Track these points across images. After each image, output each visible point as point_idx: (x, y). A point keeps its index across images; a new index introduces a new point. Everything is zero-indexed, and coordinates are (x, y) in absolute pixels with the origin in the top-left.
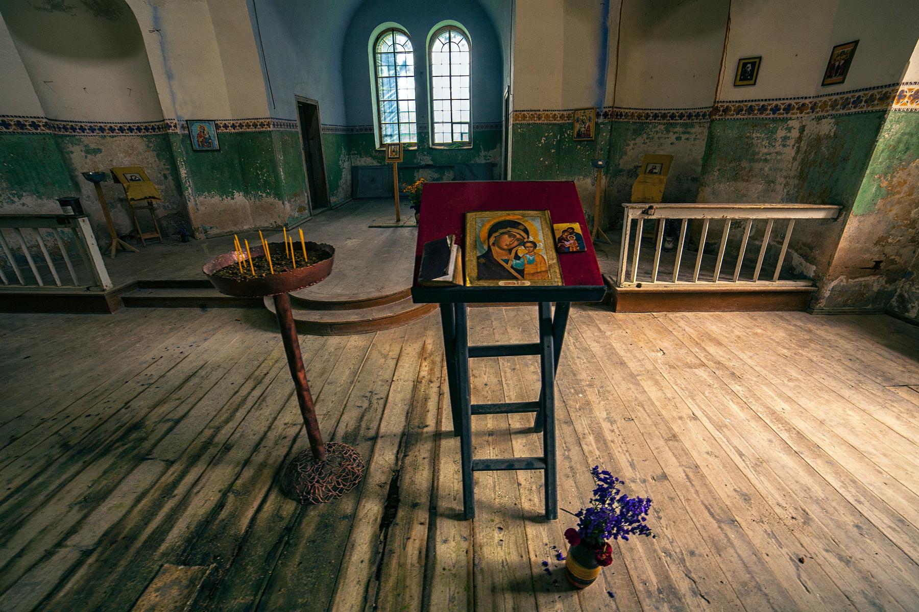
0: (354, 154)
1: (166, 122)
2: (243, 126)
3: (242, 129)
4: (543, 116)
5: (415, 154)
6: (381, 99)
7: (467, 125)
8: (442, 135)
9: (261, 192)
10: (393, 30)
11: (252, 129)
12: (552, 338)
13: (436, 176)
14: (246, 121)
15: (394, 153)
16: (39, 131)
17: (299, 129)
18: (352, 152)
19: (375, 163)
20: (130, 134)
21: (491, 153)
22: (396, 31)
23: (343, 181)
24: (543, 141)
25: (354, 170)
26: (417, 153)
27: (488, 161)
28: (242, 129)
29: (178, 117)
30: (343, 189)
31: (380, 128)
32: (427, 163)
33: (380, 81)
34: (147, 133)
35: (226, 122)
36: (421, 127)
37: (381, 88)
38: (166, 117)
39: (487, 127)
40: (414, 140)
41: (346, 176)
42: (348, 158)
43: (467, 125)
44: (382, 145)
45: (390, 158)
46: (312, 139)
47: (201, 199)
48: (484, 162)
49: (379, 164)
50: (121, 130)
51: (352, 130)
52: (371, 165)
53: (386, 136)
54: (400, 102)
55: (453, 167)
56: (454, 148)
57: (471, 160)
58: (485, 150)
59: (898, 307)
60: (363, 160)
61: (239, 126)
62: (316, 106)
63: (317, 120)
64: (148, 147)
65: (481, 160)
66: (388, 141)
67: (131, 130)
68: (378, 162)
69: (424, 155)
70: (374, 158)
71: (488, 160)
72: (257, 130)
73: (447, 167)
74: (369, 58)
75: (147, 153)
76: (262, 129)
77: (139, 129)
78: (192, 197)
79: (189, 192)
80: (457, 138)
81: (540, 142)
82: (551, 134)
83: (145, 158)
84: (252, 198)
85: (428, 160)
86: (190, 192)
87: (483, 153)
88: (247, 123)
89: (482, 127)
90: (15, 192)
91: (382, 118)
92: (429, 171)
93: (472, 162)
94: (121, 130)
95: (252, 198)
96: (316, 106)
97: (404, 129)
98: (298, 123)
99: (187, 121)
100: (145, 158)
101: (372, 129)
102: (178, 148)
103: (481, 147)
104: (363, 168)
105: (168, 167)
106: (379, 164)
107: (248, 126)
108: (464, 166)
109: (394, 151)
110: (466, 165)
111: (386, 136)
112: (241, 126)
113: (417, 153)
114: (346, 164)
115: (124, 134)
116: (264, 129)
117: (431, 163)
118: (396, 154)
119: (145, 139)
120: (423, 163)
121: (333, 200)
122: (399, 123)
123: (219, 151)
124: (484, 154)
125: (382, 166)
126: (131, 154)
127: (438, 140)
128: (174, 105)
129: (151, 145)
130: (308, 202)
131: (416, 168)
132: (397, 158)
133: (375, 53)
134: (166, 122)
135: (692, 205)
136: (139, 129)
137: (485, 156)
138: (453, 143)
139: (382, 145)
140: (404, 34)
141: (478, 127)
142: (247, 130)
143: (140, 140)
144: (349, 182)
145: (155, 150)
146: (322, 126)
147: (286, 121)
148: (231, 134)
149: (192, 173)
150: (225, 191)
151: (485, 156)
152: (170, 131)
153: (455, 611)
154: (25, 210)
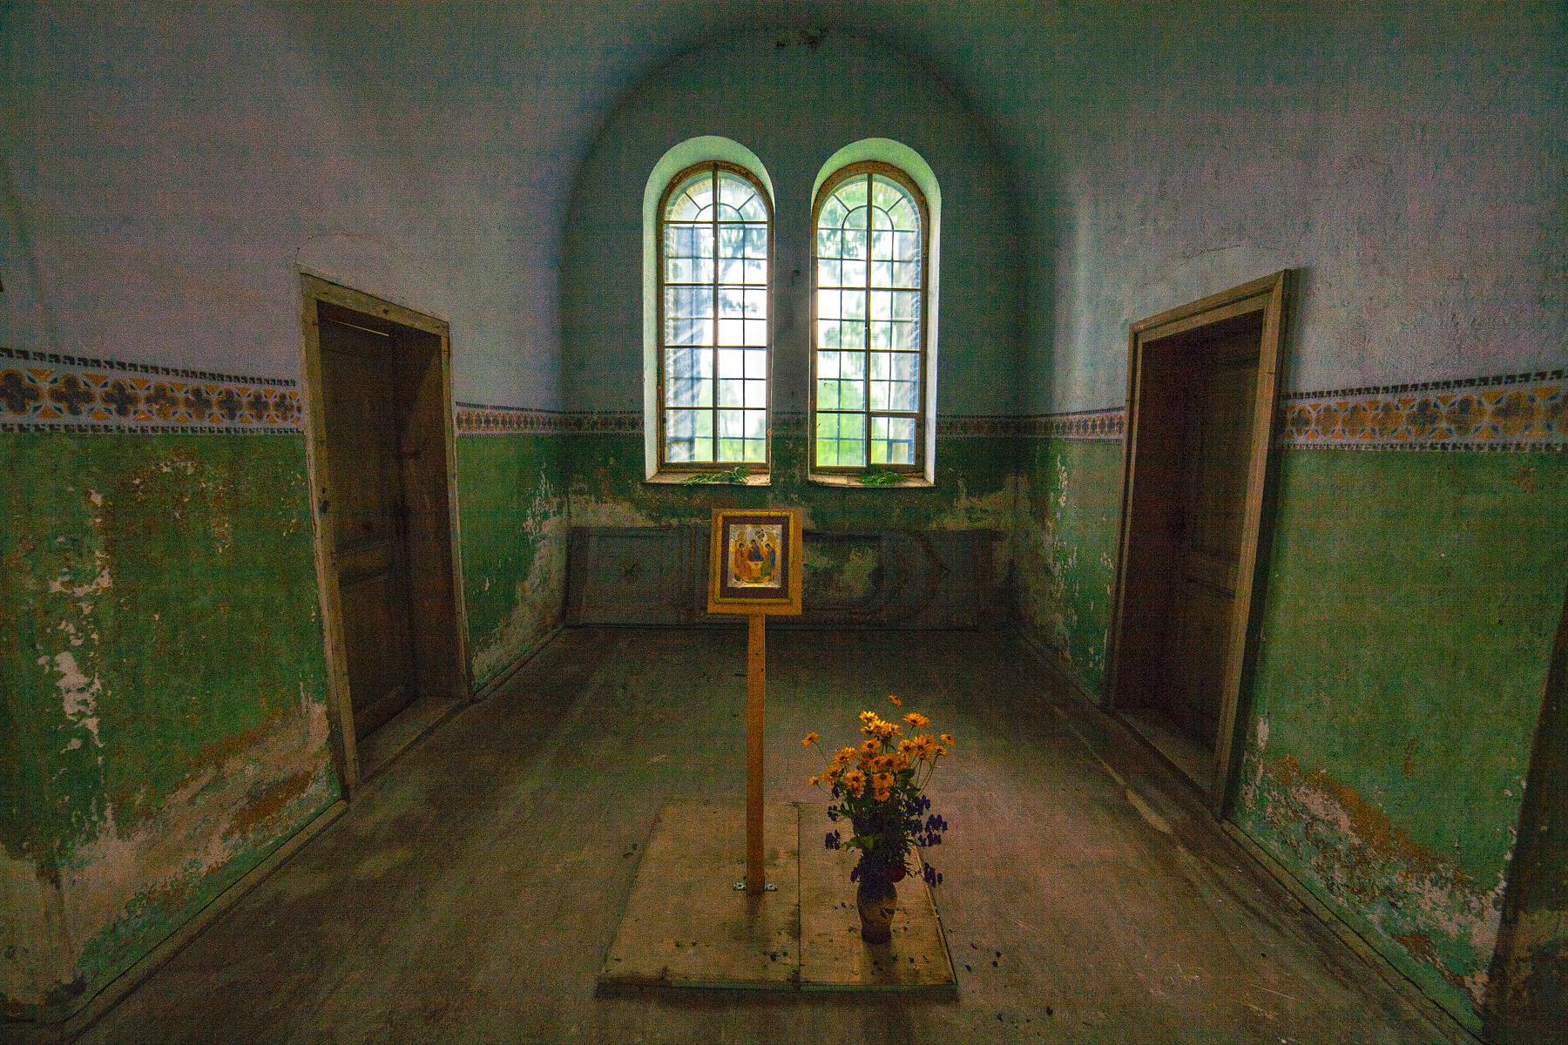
0: (581, 492)
4: (1444, 409)
6: (670, 340)
10: (716, 167)
12: (777, 586)
17: (306, 422)
18: (576, 486)
19: (641, 521)
21: (988, 502)
22: (724, 168)
23: (534, 579)
25: (577, 539)
27: (978, 525)
30: (533, 606)
31: (662, 420)
33: (670, 294)
35: (80, 373)
37: (670, 313)
40: (757, 454)
41: (548, 559)
42: (560, 506)
44: (664, 467)
46: (415, 455)
48: (964, 525)
49: (651, 524)
51: (579, 423)
52: (628, 525)
53: (677, 440)
54: (720, 352)
55: (878, 538)
57: (928, 519)
58: (969, 494)
60: (605, 509)
62: (438, 338)
63: (439, 388)
65: (954, 522)
66: (679, 455)
68: (650, 516)
70: (638, 505)
71: (979, 519)
74: (645, 264)
80: (880, 456)
87: (964, 502)
89: (965, 427)
91: (670, 394)
96: (438, 338)
97: (730, 425)
98: (304, 393)
101: (638, 423)
103: (960, 483)
104: (607, 533)
106: (651, 524)
109: (755, 555)
110: (919, 535)
111: (677, 440)
114: (551, 526)
118: (766, 573)
121: (484, 662)
122: (715, 409)
124: (968, 504)
125: (661, 529)
127: (826, 456)
128: (839, 429)
130: (335, 739)
133: (660, 223)
137: (970, 511)
138: (871, 470)
139: (664, 467)
140: (747, 175)
141: (951, 426)
144: (555, 583)
146: (456, 410)
151: (970, 511)
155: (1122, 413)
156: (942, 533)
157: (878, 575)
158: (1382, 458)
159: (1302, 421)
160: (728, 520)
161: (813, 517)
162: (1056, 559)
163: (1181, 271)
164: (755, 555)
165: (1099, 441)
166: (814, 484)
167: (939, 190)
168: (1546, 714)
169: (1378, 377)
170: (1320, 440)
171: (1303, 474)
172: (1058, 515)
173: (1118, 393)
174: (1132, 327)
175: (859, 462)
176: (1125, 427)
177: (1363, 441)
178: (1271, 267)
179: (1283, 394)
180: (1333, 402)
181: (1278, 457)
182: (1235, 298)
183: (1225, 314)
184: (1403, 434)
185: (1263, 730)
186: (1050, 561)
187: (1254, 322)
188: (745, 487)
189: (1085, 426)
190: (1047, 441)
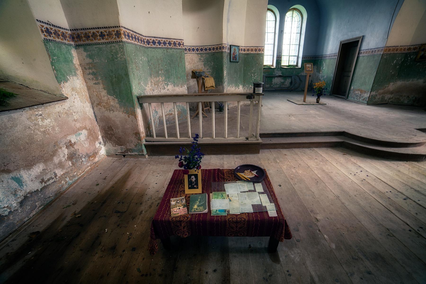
1: (223, 45)
2: (249, 50)
3: (248, 51)
5: (274, 70)
7: (296, 57)
8: (285, 63)
9: (251, 86)
11: (254, 52)
13: (282, 81)
14: (251, 48)
15: (309, 68)
16: (166, 46)
20: (193, 52)
24: (395, 62)
26: (275, 70)
28: (248, 51)
29: (227, 43)
32: (279, 75)
34: (201, 52)
36: (278, 57)
38: (224, 43)
39: (309, 58)
43: (296, 57)
45: (307, 71)
47: (229, 88)
50: (189, 50)
55: (291, 77)
56: (292, 69)
57: (299, 73)
59: (59, 177)
61: (247, 50)
64: (200, 59)
67: (193, 50)
69: (278, 71)
72: (256, 52)
73: (288, 77)
75: (199, 63)
76: (259, 52)
77: (197, 50)
78: (226, 87)
79: (225, 84)
81: (393, 62)
82: (400, 58)
83: (197, 66)
84: (246, 89)
85: (280, 73)
86: (226, 84)
88: (252, 49)
89: (306, 58)
90: (166, 82)
92: (279, 78)
93: (300, 74)
94: (189, 50)
95: (246, 89)
99: (230, 46)
100: (197, 66)
102: (226, 60)
105: (210, 70)
107: (252, 50)
108: (296, 77)
109: (309, 67)
110: (298, 76)
112: (248, 50)
113: (275, 70)
115: (190, 52)
116: (260, 52)
117: (281, 75)
119: (199, 55)
120: (277, 75)
123: (238, 62)
126: (191, 63)
129: (202, 58)
131: (273, 77)
132: (310, 71)
134: (223, 45)
135: (342, 97)
136: (197, 50)
141: (304, 58)
142: (251, 52)
143: (196, 55)
145: (203, 61)
147: (135, 34)
148: (243, 54)
149: (228, 74)
150: (237, 86)
152: (224, 50)
153: (356, 279)
154: (168, 93)
155: (337, 54)
156: (301, 75)
157: (291, 83)
158: (368, 56)
159: (361, 53)
160: (311, 64)
161: (282, 73)
162: (322, 78)
163: (349, 34)
164: (309, 67)
165: (332, 58)
166: (282, 68)
167: (375, 73)
168: (376, 76)
169: (369, 48)
170: (363, 55)
171: (361, 59)
172: (323, 71)
173: (337, 51)
174: (340, 41)
175: (288, 65)
176: (337, 56)
177: (367, 55)
178: (361, 35)
179: (360, 50)
180: (365, 51)
181: (358, 57)
182: (356, 38)
183: (355, 40)
184: (371, 54)
185: (352, 88)
186: (321, 78)
187: (358, 41)
188: (271, 68)
189: (330, 56)
190: (321, 59)
